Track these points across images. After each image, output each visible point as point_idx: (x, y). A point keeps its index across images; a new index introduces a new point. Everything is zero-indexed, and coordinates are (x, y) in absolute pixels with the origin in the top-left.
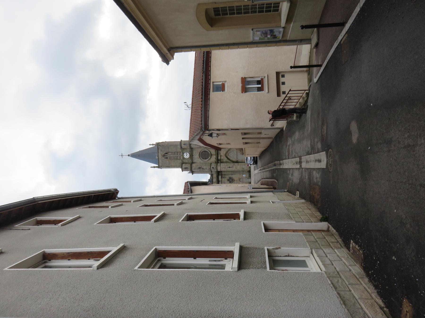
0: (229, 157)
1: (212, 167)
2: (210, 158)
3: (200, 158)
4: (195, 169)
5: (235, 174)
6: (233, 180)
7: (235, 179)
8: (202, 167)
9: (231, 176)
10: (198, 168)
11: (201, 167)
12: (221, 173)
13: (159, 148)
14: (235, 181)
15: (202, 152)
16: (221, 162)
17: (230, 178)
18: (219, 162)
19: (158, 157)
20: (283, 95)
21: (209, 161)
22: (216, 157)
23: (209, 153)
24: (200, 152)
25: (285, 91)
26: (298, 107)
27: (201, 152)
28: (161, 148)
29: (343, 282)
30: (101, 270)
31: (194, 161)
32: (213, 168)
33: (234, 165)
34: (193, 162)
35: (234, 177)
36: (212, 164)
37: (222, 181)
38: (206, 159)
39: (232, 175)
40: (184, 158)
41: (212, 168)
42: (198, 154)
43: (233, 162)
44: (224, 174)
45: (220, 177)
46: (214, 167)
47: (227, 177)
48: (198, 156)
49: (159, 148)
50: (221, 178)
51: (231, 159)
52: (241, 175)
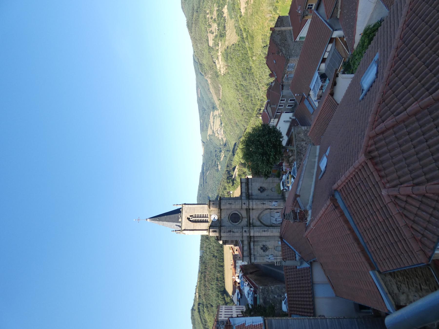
0: (261, 220)
1: (244, 230)
2: (240, 221)
3: (229, 221)
4: (225, 232)
5: (269, 241)
6: (267, 248)
7: (270, 247)
8: (233, 230)
9: (264, 243)
10: (228, 231)
11: (231, 230)
12: (254, 238)
13: (184, 209)
14: (270, 249)
15: (232, 215)
16: (253, 226)
17: (264, 246)
18: (251, 226)
19: (181, 219)
20: (200, 238)
21: (240, 224)
22: (247, 220)
23: (240, 215)
24: (230, 215)
25: (201, 235)
26: (218, 233)
27: (231, 215)
28: (186, 209)
29: (204, 312)
30: (156, 223)
31: (223, 224)
32: (245, 231)
33: (269, 228)
34: (222, 225)
35: (268, 245)
36: (244, 227)
37: (254, 249)
38: (236, 222)
39: (266, 242)
40: (241, 197)
41: (244, 232)
42: (228, 217)
43: (267, 226)
44: (257, 241)
45: (252, 244)
46: (246, 230)
47: (261, 245)
48: (228, 219)
49: (184, 209)
50: (254, 245)
51: (264, 223)
52: (277, 242)
